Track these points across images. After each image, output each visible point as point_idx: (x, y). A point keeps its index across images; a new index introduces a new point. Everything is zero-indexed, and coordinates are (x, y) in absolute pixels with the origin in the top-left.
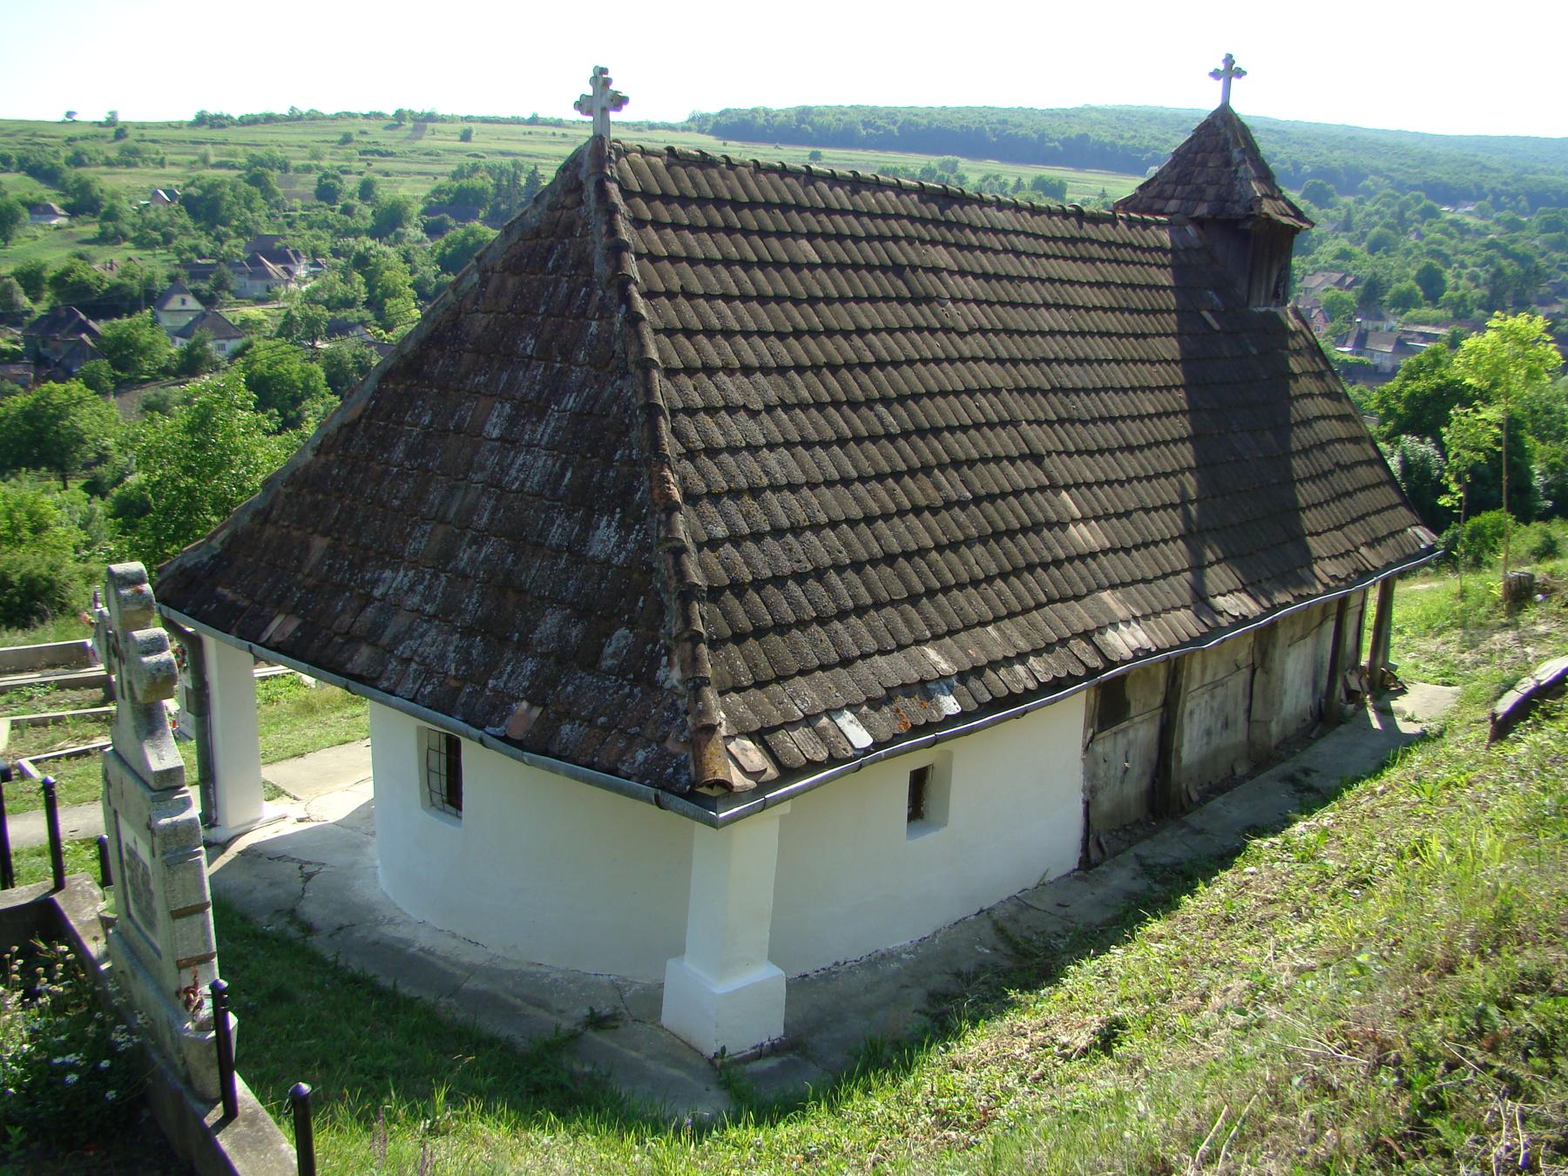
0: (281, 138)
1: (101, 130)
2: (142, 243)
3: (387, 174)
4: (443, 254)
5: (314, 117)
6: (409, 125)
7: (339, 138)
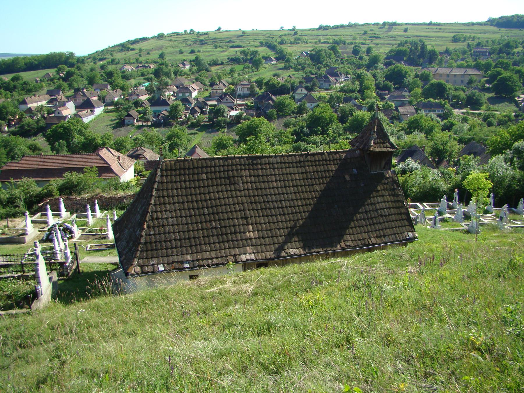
0: (344, 33)
1: (290, 32)
2: (296, 70)
3: (377, 45)
4: (386, 74)
5: (356, 25)
6: (387, 27)
7: (363, 32)
